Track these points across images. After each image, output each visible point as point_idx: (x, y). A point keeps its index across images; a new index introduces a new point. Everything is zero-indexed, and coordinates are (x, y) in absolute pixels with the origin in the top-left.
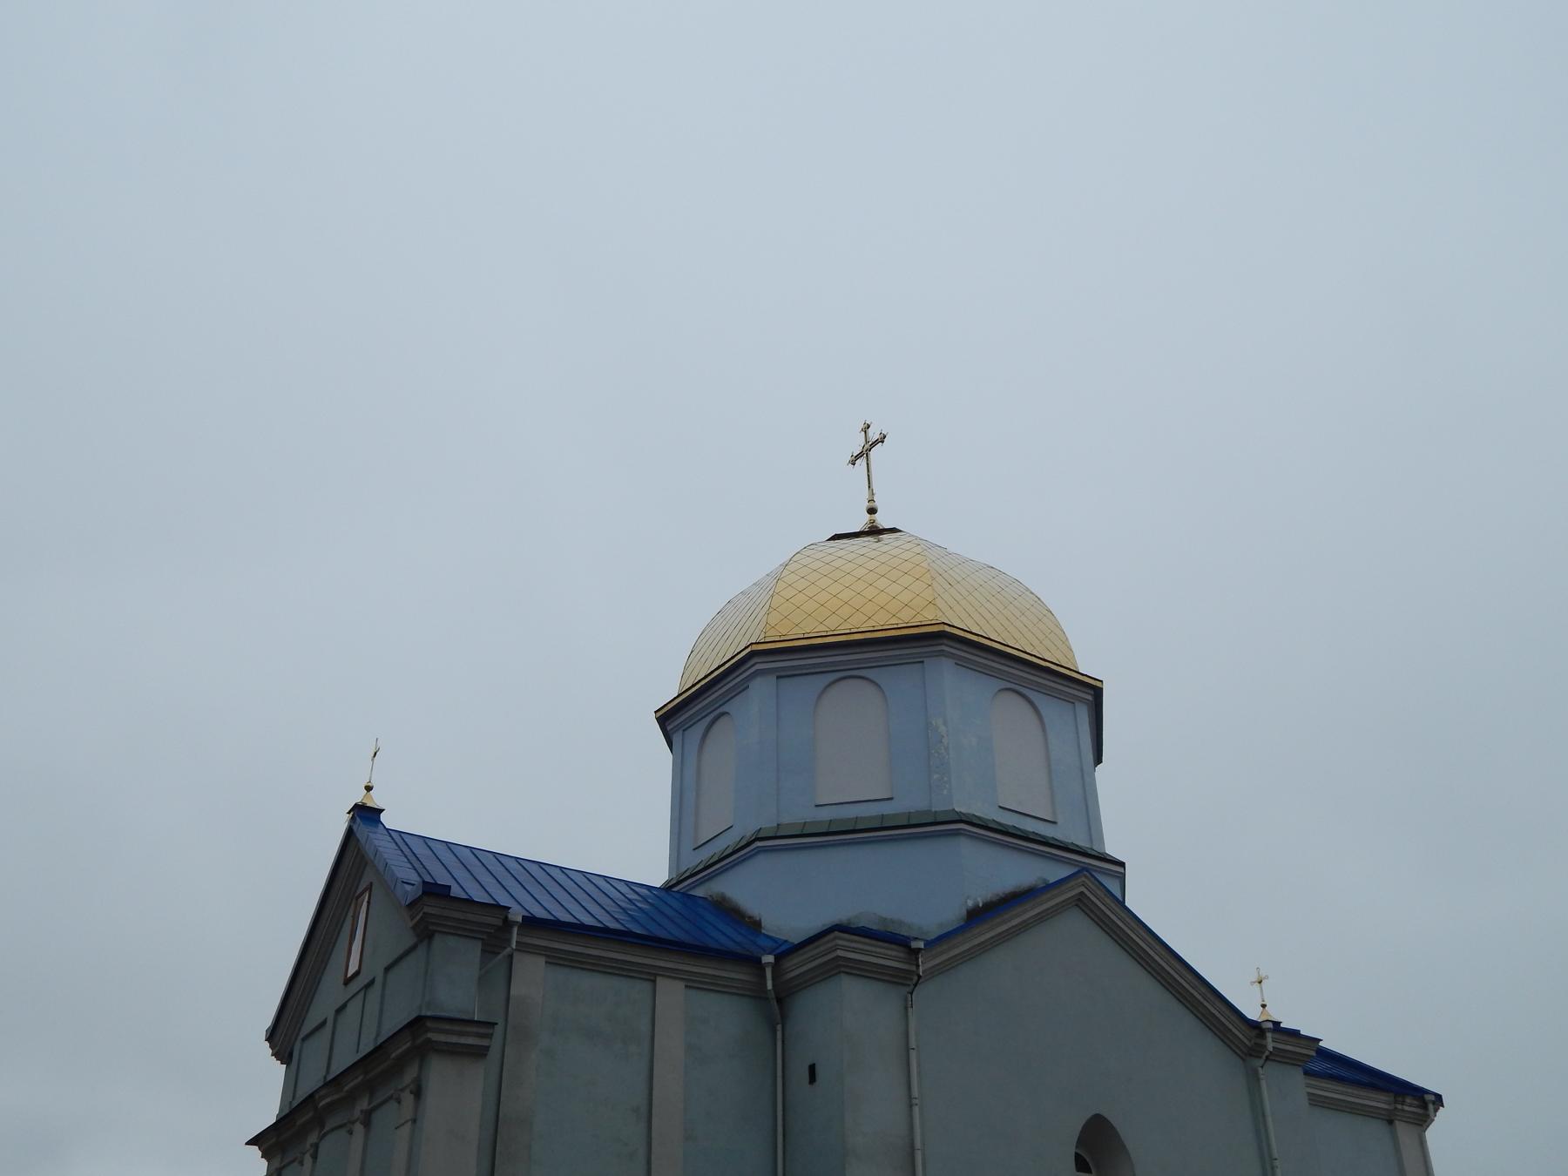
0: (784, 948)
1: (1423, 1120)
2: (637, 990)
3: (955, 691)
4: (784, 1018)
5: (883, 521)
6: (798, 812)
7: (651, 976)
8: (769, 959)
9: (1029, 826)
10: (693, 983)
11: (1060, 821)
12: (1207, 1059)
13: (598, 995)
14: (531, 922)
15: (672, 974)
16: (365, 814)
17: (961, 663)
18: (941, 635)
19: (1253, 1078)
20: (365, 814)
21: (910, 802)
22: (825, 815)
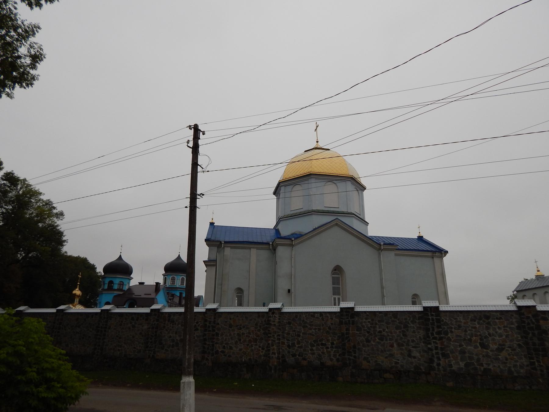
0: (356, 225)
1: (442, 257)
2: (247, 251)
3: (314, 186)
4: (275, 253)
5: (321, 145)
6: (289, 213)
7: (250, 248)
8: (271, 243)
9: (332, 209)
10: (257, 249)
11: (340, 207)
12: (368, 252)
13: (240, 252)
14: (225, 242)
15: (253, 248)
16: (212, 224)
17: (316, 179)
18: (309, 176)
19: (380, 254)
20: (212, 224)
21: (305, 209)
22: (292, 212)
